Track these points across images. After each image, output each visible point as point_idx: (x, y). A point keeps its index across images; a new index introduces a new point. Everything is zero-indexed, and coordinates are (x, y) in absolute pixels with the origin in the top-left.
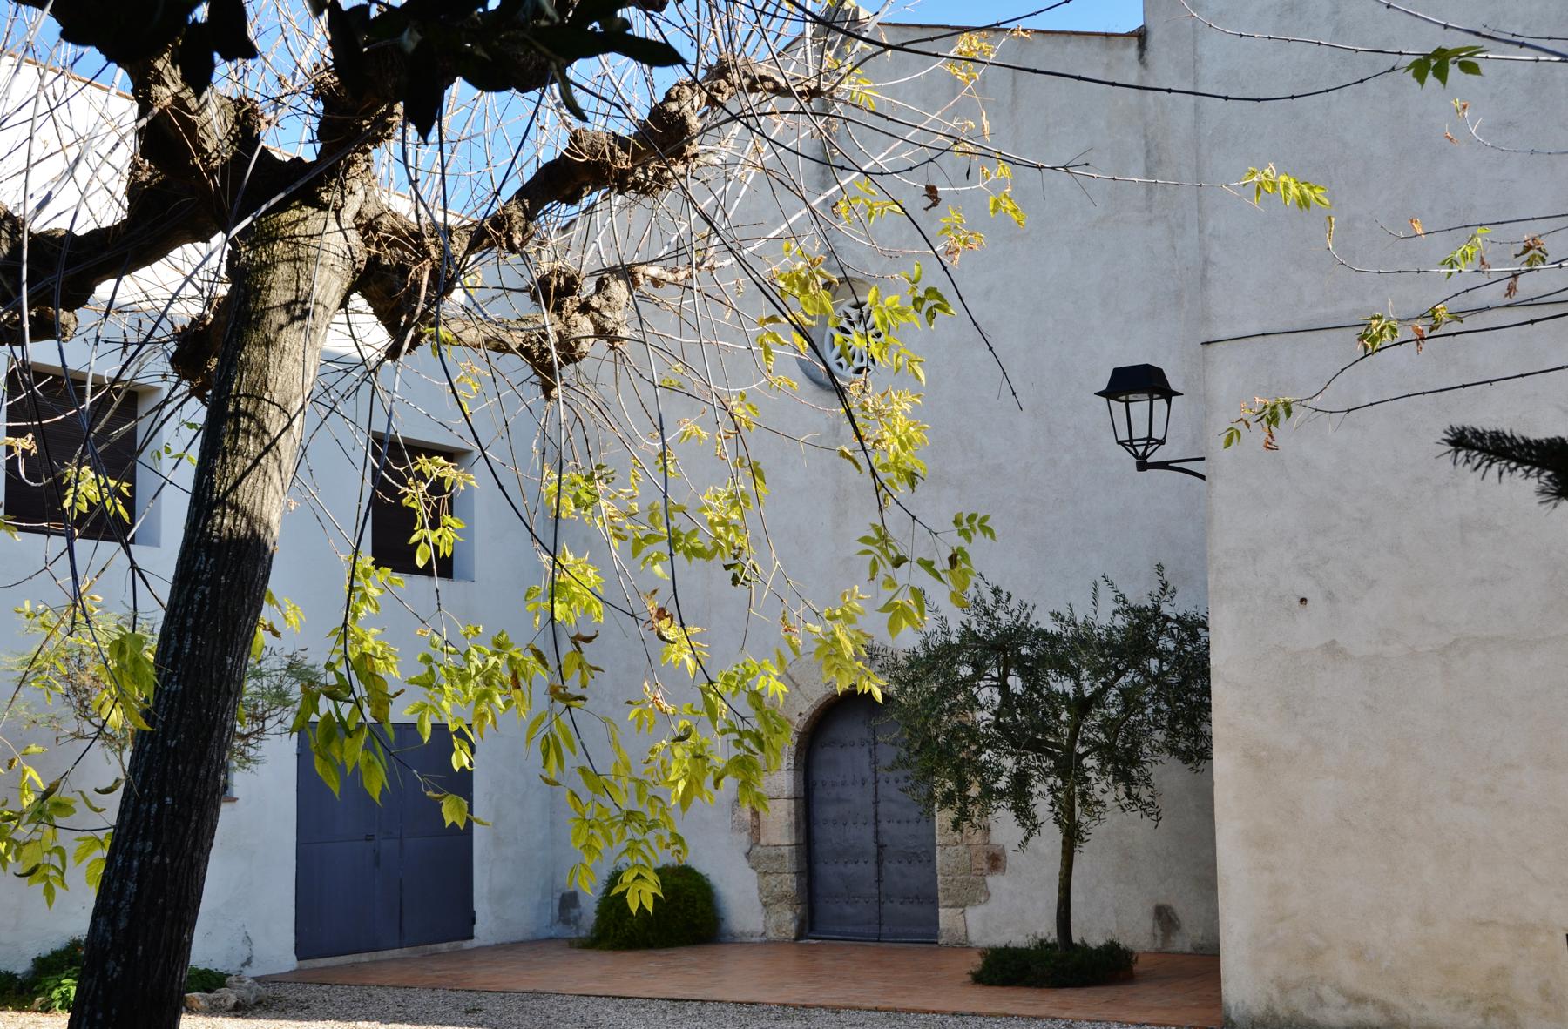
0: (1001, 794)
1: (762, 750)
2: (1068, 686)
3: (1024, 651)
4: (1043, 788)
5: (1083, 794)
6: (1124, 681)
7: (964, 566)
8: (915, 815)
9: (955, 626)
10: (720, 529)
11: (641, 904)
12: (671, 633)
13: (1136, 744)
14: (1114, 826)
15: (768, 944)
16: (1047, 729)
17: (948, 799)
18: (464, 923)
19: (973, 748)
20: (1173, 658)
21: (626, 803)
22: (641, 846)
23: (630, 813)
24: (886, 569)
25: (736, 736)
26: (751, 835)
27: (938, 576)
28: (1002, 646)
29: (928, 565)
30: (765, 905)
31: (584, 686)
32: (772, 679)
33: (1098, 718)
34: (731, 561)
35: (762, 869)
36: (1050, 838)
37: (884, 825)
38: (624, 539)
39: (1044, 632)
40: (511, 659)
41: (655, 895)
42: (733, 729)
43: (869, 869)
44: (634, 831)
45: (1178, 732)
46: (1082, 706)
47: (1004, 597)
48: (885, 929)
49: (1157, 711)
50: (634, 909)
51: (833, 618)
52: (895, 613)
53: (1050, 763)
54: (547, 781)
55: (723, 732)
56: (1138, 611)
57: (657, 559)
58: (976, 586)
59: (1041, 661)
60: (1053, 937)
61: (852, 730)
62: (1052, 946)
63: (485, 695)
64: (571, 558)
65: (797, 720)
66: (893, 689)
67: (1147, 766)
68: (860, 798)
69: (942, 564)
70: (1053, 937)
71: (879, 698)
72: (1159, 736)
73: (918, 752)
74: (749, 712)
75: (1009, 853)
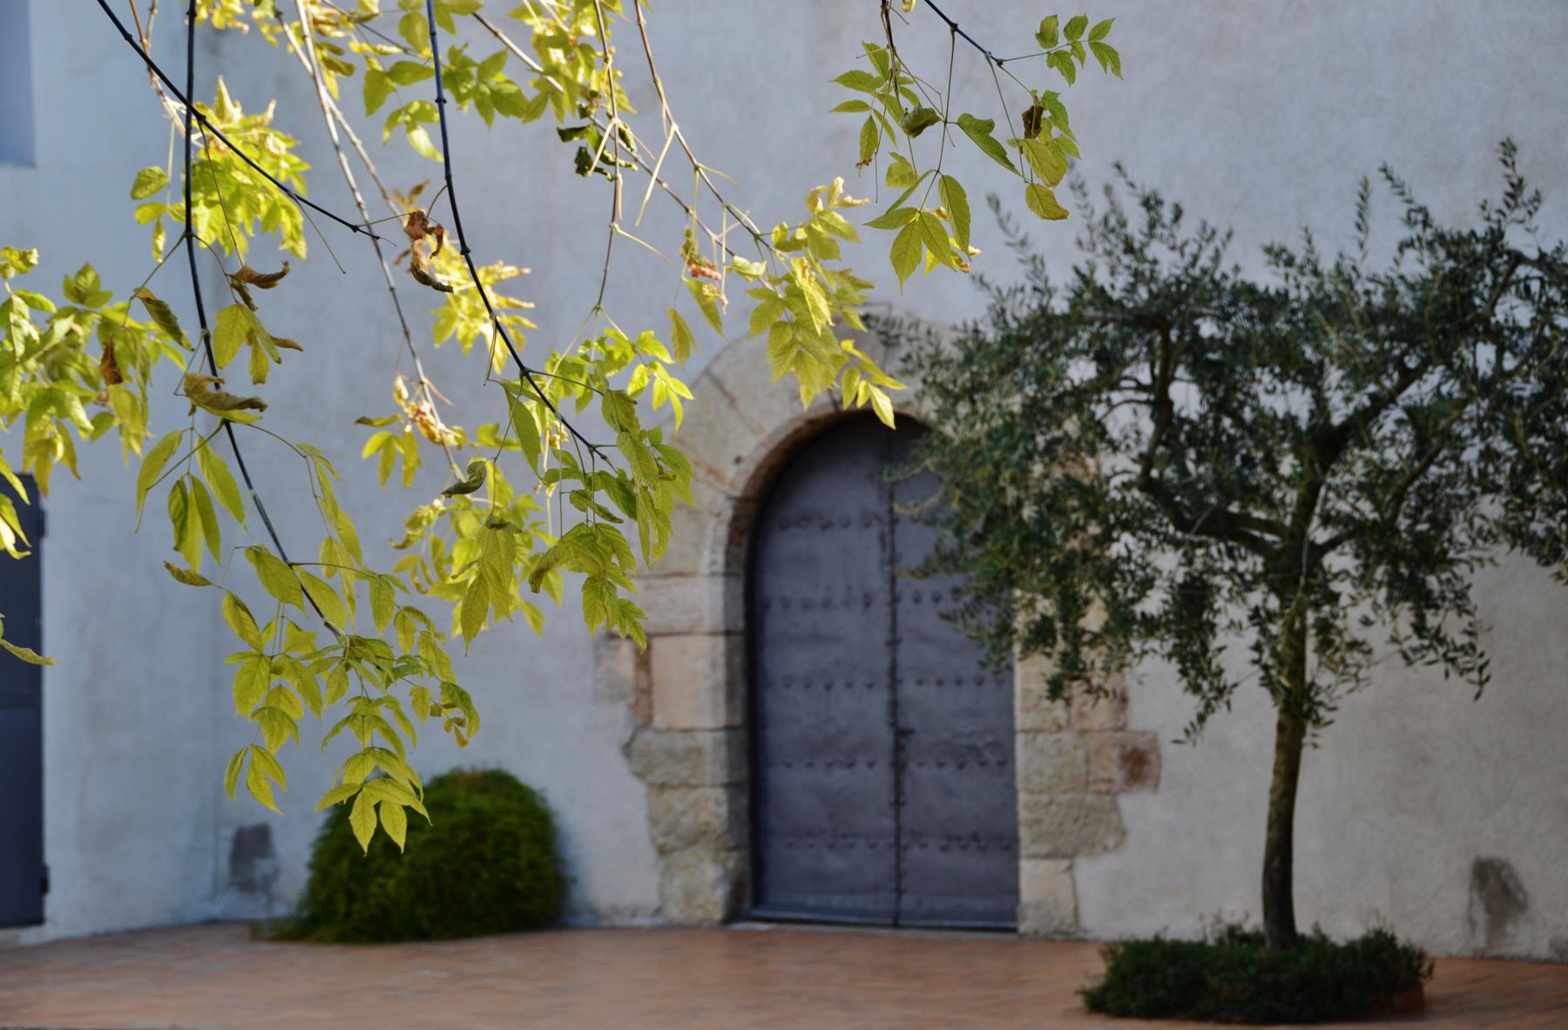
0: (1150, 626)
1: (632, 514)
2: (1293, 402)
3: (1207, 329)
4: (1239, 613)
5: (1324, 627)
6: (1420, 392)
7: (1055, 132)
8: (972, 669)
9: (1062, 280)
10: (557, 55)
11: (379, 830)
12: (451, 272)
13: (1441, 524)
14: (1382, 686)
15: (669, 931)
16: (1250, 493)
17: (1041, 635)
19: (1094, 529)
20: (1528, 341)
21: (350, 622)
22: (383, 712)
23: (357, 642)
24: (895, 142)
25: (579, 485)
26: (634, 707)
27: (1001, 156)
28: (1158, 321)
29: (980, 130)
30: (662, 851)
31: (259, 380)
32: (660, 372)
33: (1359, 469)
34: (572, 121)
35: (658, 776)
36: (1253, 715)
37: (909, 690)
38: (349, 70)
39: (1250, 290)
40: (106, 325)
41: (408, 809)
42: (572, 471)
43: (878, 779)
44: (363, 681)
45: (1531, 500)
46: (1326, 443)
47: (1167, 214)
48: (908, 902)
49: (1489, 455)
50: (364, 840)
51: (790, 245)
52: (908, 232)
53: (1253, 563)
54: (181, 576)
55: (552, 477)
56: (1454, 244)
57: (418, 118)
58: (1108, 190)
59: (1240, 349)
60: (1254, 920)
61: (843, 494)
62: (1252, 940)
63: (48, 400)
64: (235, 113)
65: (731, 472)
66: (928, 408)
67: (1461, 570)
68: (859, 632)
69: (1008, 129)
70: (1254, 920)
71: (888, 418)
72: (1491, 508)
73: (979, 539)
74: (602, 432)
75: (1168, 750)
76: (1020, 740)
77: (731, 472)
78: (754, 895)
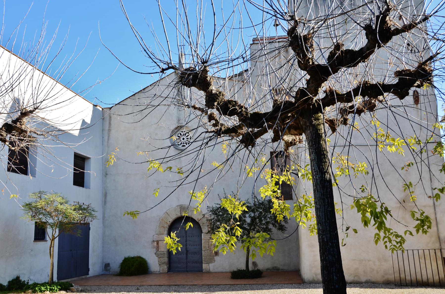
18: (87, 270)
30: (160, 265)
35: (159, 256)
37: (188, 246)
48: (188, 269)
60: (245, 269)
70: (245, 269)
76: (203, 251)
77: (169, 223)
78: (170, 269)
